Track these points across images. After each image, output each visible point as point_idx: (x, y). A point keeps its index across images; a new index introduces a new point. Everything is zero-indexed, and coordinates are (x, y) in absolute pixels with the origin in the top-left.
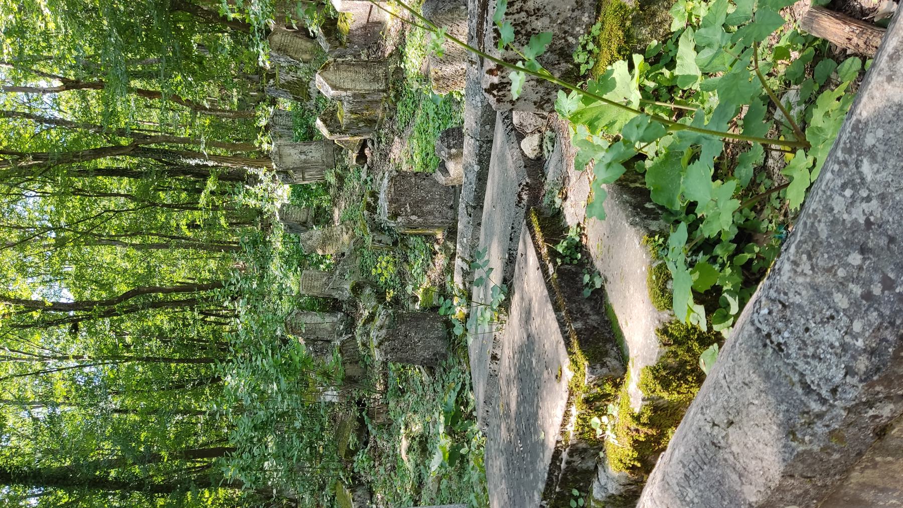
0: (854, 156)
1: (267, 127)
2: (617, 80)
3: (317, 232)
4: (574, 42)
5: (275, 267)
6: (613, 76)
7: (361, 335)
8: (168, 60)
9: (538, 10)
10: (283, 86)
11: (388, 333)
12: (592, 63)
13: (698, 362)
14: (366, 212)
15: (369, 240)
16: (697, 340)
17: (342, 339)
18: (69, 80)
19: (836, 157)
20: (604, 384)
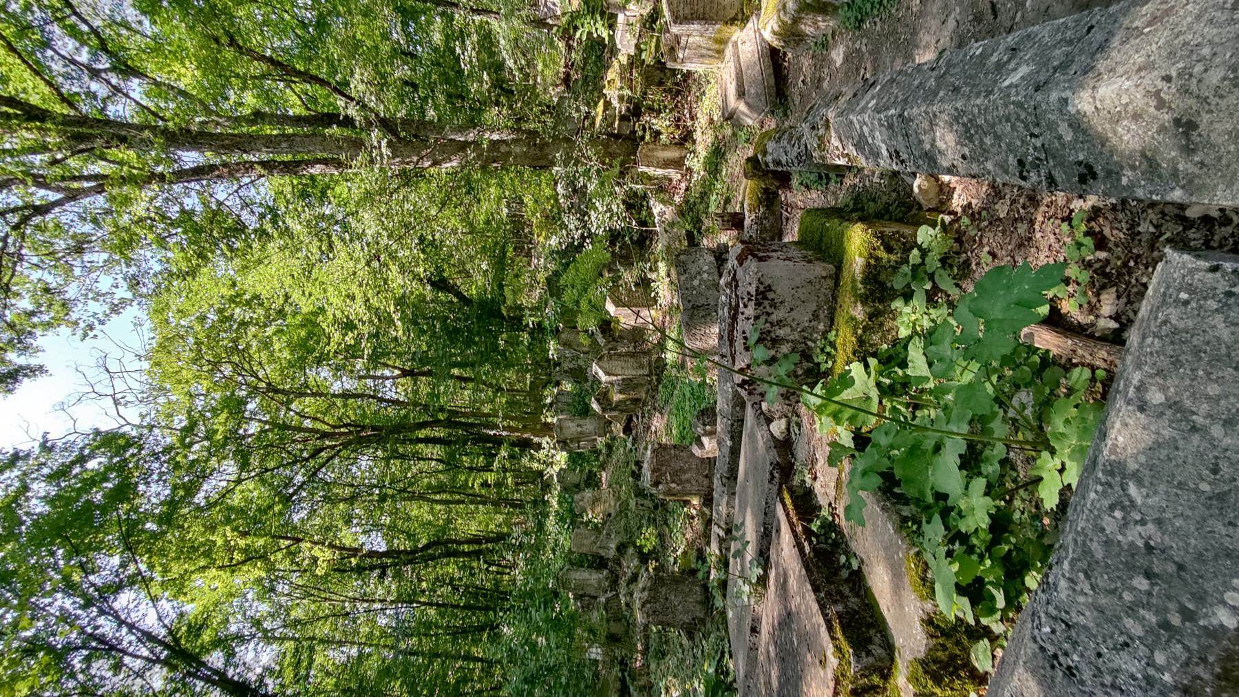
0: (1118, 479)
1: (551, 404)
2: (855, 377)
3: (588, 494)
4: (813, 345)
5: (551, 524)
6: (851, 374)
7: (625, 595)
8: (482, 353)
9: (781, 321)
10: (566, 372)
11: (649, 596)
12: (830, 363)
13: (969, 655)
14: (631, 479)
15: (632, 504)
16: (965, 632)
17: (607, 596)
18: (406, 370)
19: (1097, 478)
20: (871, 674)
